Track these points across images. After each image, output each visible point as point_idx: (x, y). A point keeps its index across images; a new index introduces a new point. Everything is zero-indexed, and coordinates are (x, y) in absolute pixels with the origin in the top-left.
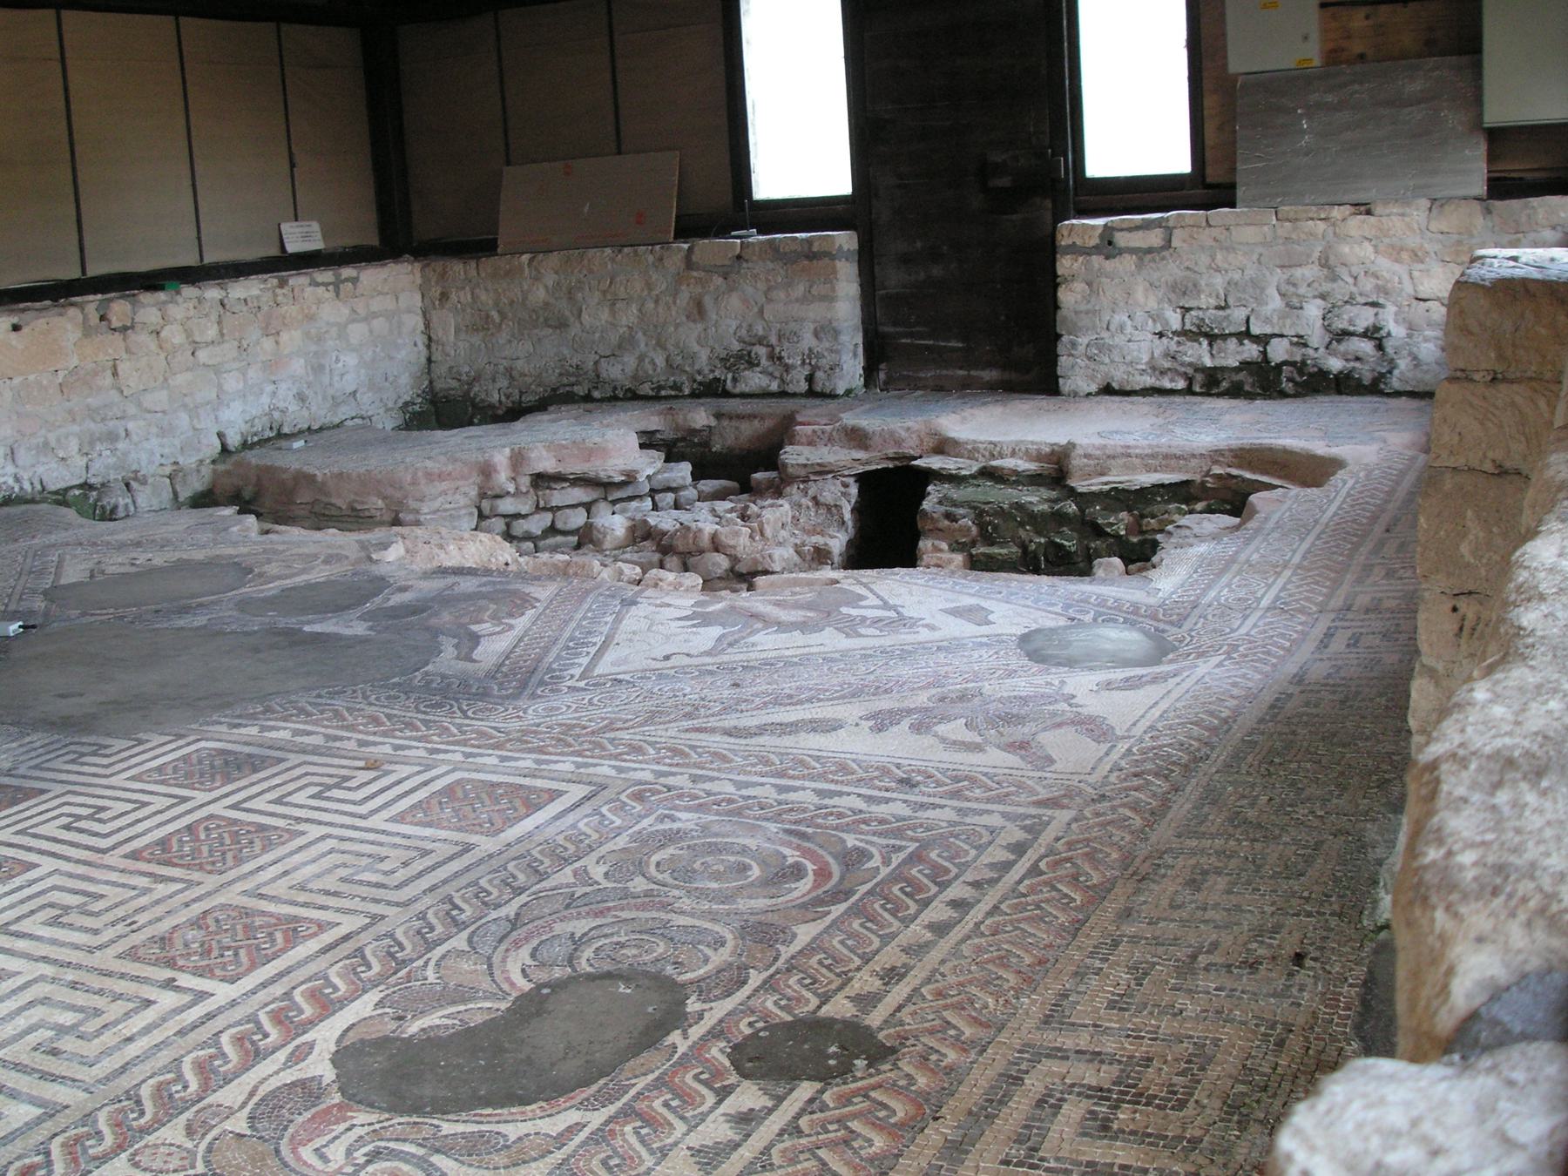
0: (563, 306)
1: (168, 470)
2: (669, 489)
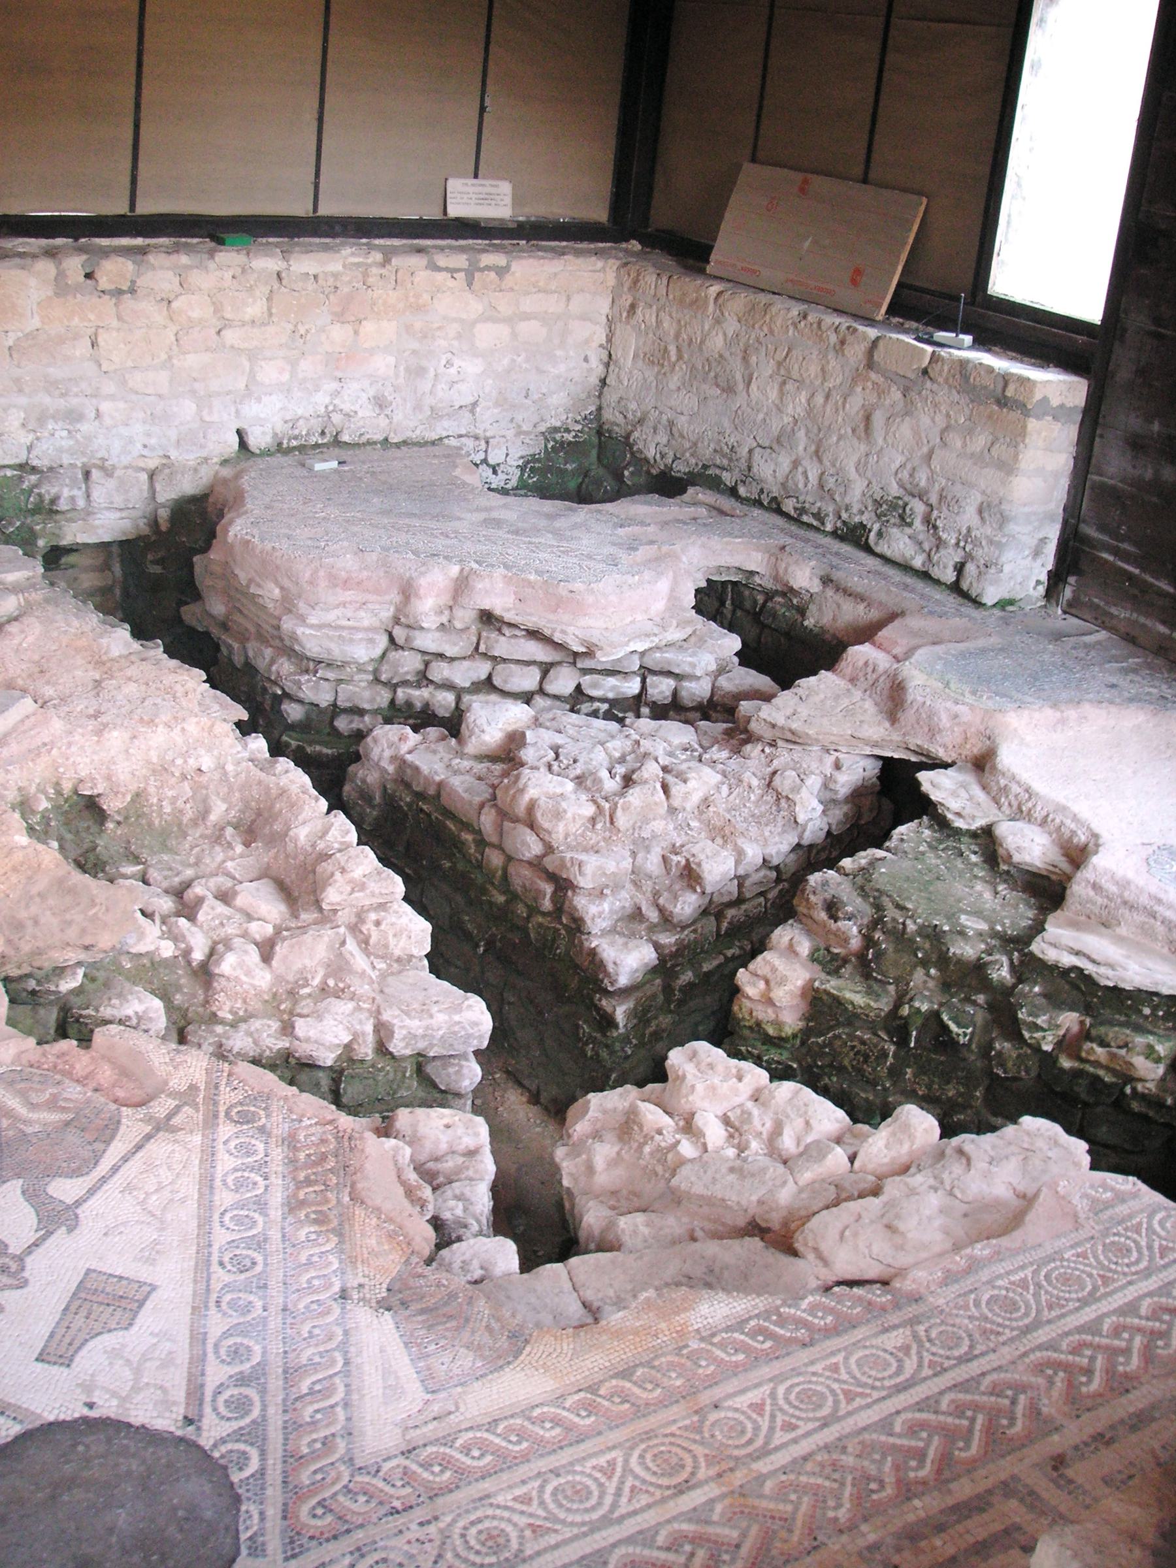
1: (152, 464)
2: (669, 674)
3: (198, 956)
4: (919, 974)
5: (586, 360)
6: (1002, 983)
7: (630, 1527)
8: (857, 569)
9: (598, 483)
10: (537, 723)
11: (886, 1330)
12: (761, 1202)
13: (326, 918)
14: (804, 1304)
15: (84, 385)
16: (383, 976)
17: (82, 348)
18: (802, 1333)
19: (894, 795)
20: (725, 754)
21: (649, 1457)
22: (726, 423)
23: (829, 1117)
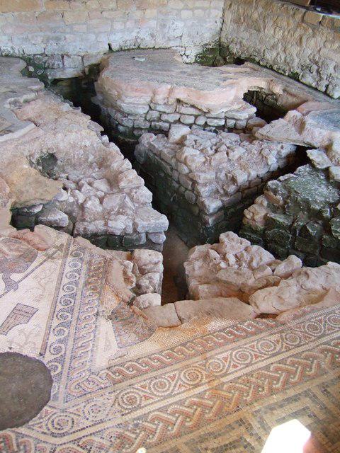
0: (261, 23)
1: (83, 54)
2: (233, 119)
3: (80, 201)
4: (301, 213)
5: (216, 22)
6: (327, 217)
7: (177, 398)
8: (295, 88)
9: (219, 61)
10: (191, 133)
11: (272, 334)
12: (242, 284)
13: (121, 191)
14: (246, 324)
15: (61, 29)
16: (137, 208)
17: (58, 18)
18: (244, 334)
19: (299, 157)
20: (247, 143)
21: (187, 374)
22: (257, 41)
23: (267, 256)
